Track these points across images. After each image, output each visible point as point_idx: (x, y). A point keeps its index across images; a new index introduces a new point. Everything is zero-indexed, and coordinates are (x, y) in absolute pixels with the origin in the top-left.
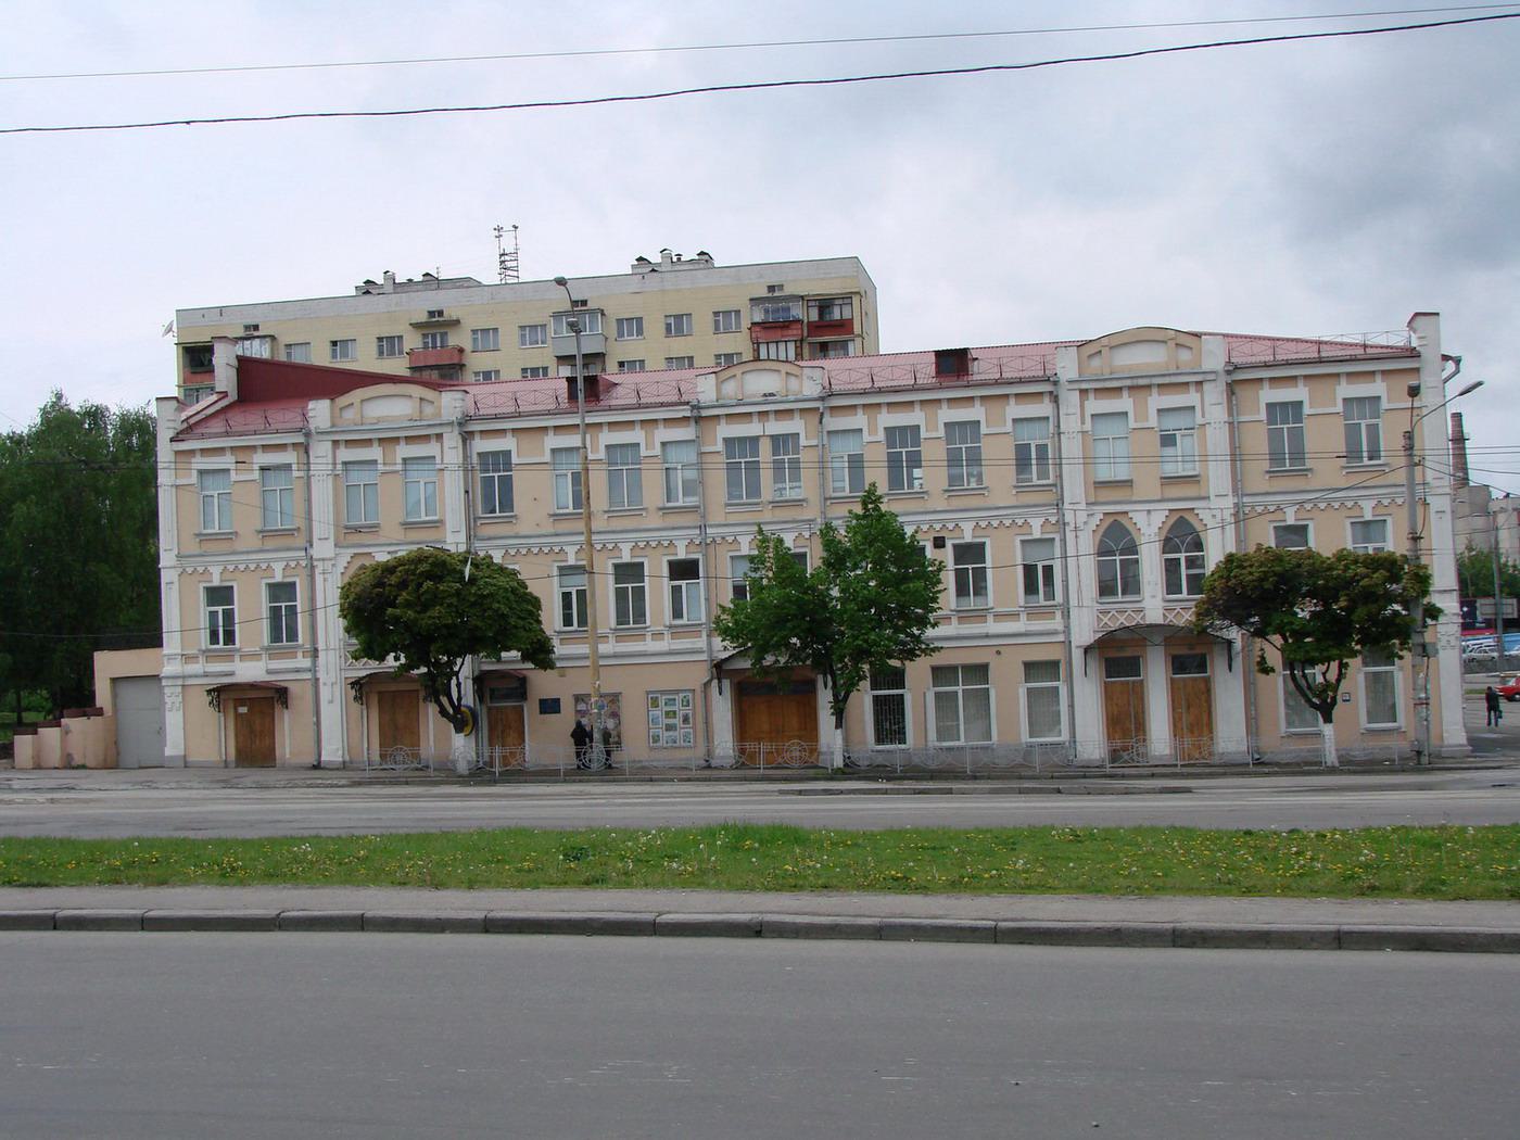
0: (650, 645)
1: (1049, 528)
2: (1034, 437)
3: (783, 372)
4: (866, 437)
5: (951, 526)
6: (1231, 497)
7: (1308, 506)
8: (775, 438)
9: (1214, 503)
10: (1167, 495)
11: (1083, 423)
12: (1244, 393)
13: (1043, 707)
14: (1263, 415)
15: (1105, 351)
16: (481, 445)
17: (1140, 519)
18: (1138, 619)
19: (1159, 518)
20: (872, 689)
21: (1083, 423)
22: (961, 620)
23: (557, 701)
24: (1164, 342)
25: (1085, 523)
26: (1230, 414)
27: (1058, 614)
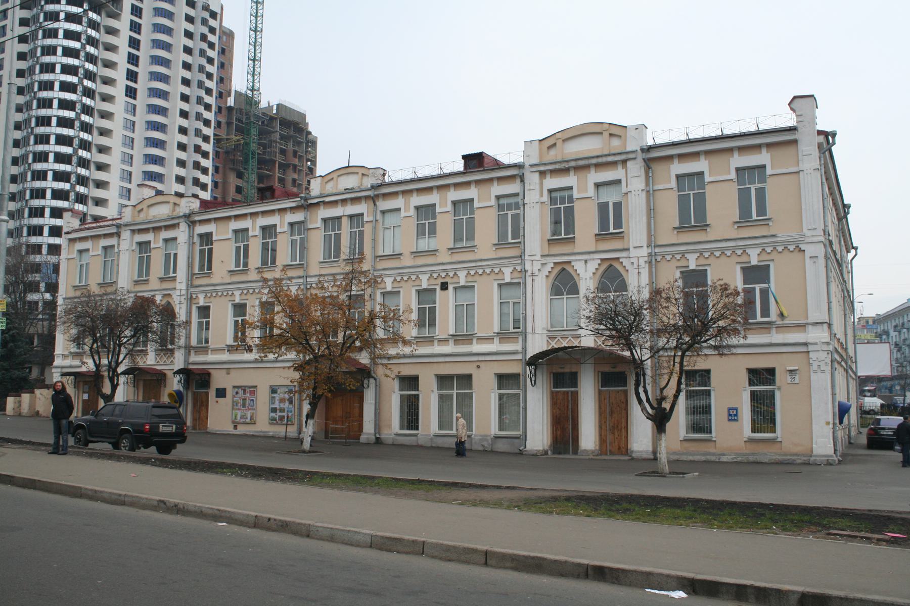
0: (438, 349)
1: (516, 275)
2: (610, 197)
3: (360, 174)
4: (403, 213)
5: (451, 274)
6: (645, 247)
7: (706, 255)
8: (351, 217)
9: (633, 253)
10: (601, 248)
11: (542, 195)
12: (658, 168)
13: (510, 408)
14: (673, 184)
15: (559, 143)
16: (201, 229)
17: (579, 266)
18: (576, 343)
19: (593, 266)
20: (750, 385)
21: (542, 195)
22: (456, 342)
23: (225, 389)
24: (601, 133)
25: (539, 270)
26: (647, 184)
27: (520, 340)
